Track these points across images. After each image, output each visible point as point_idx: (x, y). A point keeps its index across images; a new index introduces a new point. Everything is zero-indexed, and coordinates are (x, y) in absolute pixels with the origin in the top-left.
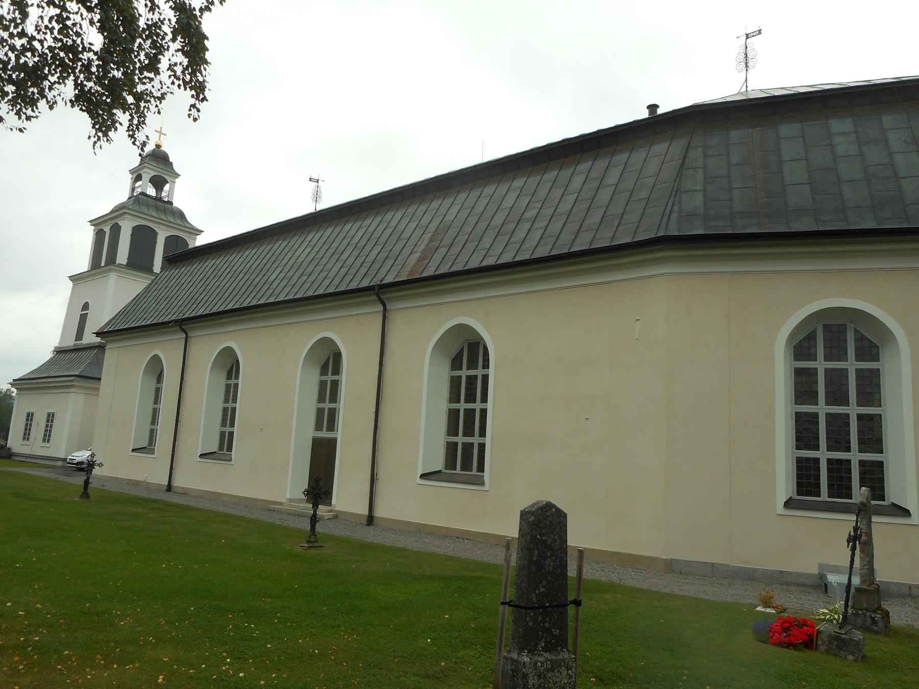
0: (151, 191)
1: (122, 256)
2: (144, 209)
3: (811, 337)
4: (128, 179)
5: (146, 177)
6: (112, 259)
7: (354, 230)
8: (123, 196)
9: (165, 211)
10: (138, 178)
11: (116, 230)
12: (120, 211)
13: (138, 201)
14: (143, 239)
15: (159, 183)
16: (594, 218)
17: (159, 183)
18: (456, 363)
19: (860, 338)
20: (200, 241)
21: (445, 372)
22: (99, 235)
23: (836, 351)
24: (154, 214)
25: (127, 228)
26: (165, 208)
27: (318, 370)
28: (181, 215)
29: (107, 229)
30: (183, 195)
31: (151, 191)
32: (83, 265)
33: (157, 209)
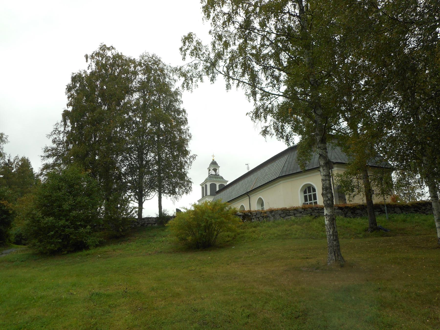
0: (214, 173)
1: (209, 193)
2: (212, 179)
3: (306, 190)
4: (207, 171)
5: (211, 170)
6: (206, 195)
7: (259, 173)
8: (207, 176)
9: (217, 178)
10: (210, 170)
11: (206, 186)
12: (206, 181)
13: (211, 176)
14: (213, 186)
15: (215, 170)
16: (285, 168)
17: (215, 170)
18: (305, 192)
19: (312, 188)
20: (228, 183)
21: (303, 195)
22: (203, 188)
23: (310, 192)
24: (215, 179)
25: (208, 185)
26: (217, 176)
27: (303, 193)
28: (222, 178)
29: (204, 186)
30: (221, 172)
31: (214, 173)
32: (200, 197)
33: (215, 178)
